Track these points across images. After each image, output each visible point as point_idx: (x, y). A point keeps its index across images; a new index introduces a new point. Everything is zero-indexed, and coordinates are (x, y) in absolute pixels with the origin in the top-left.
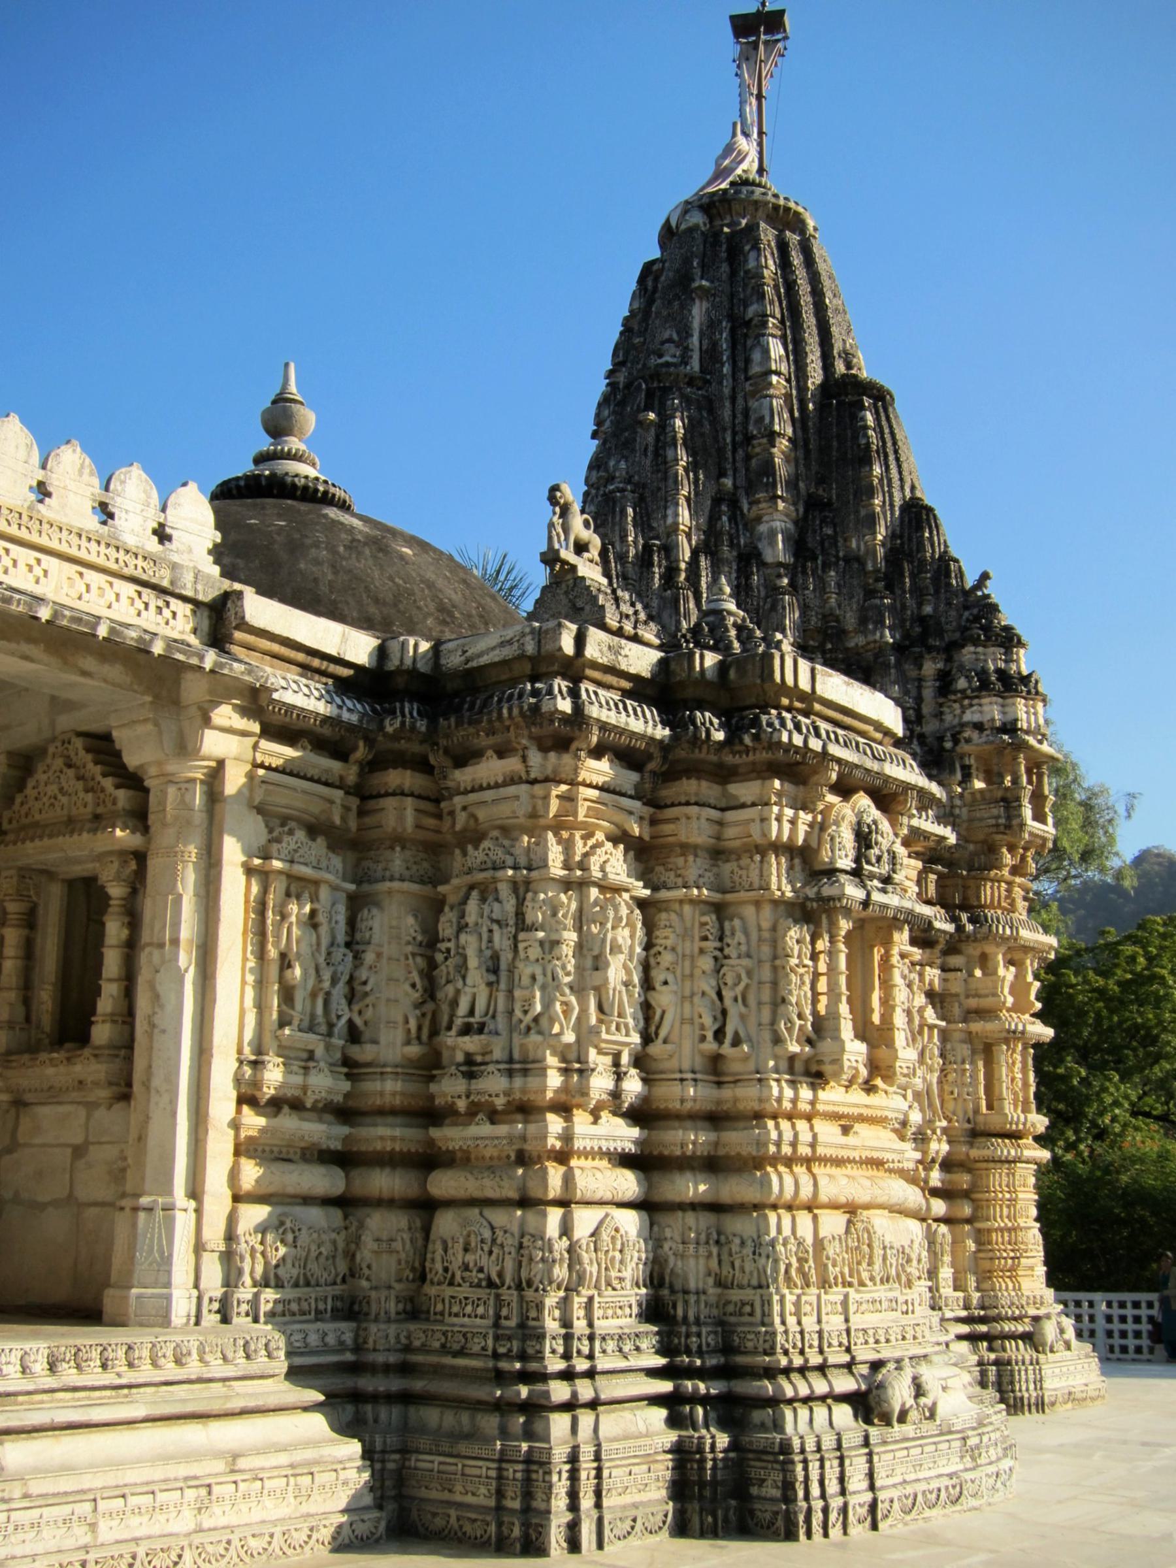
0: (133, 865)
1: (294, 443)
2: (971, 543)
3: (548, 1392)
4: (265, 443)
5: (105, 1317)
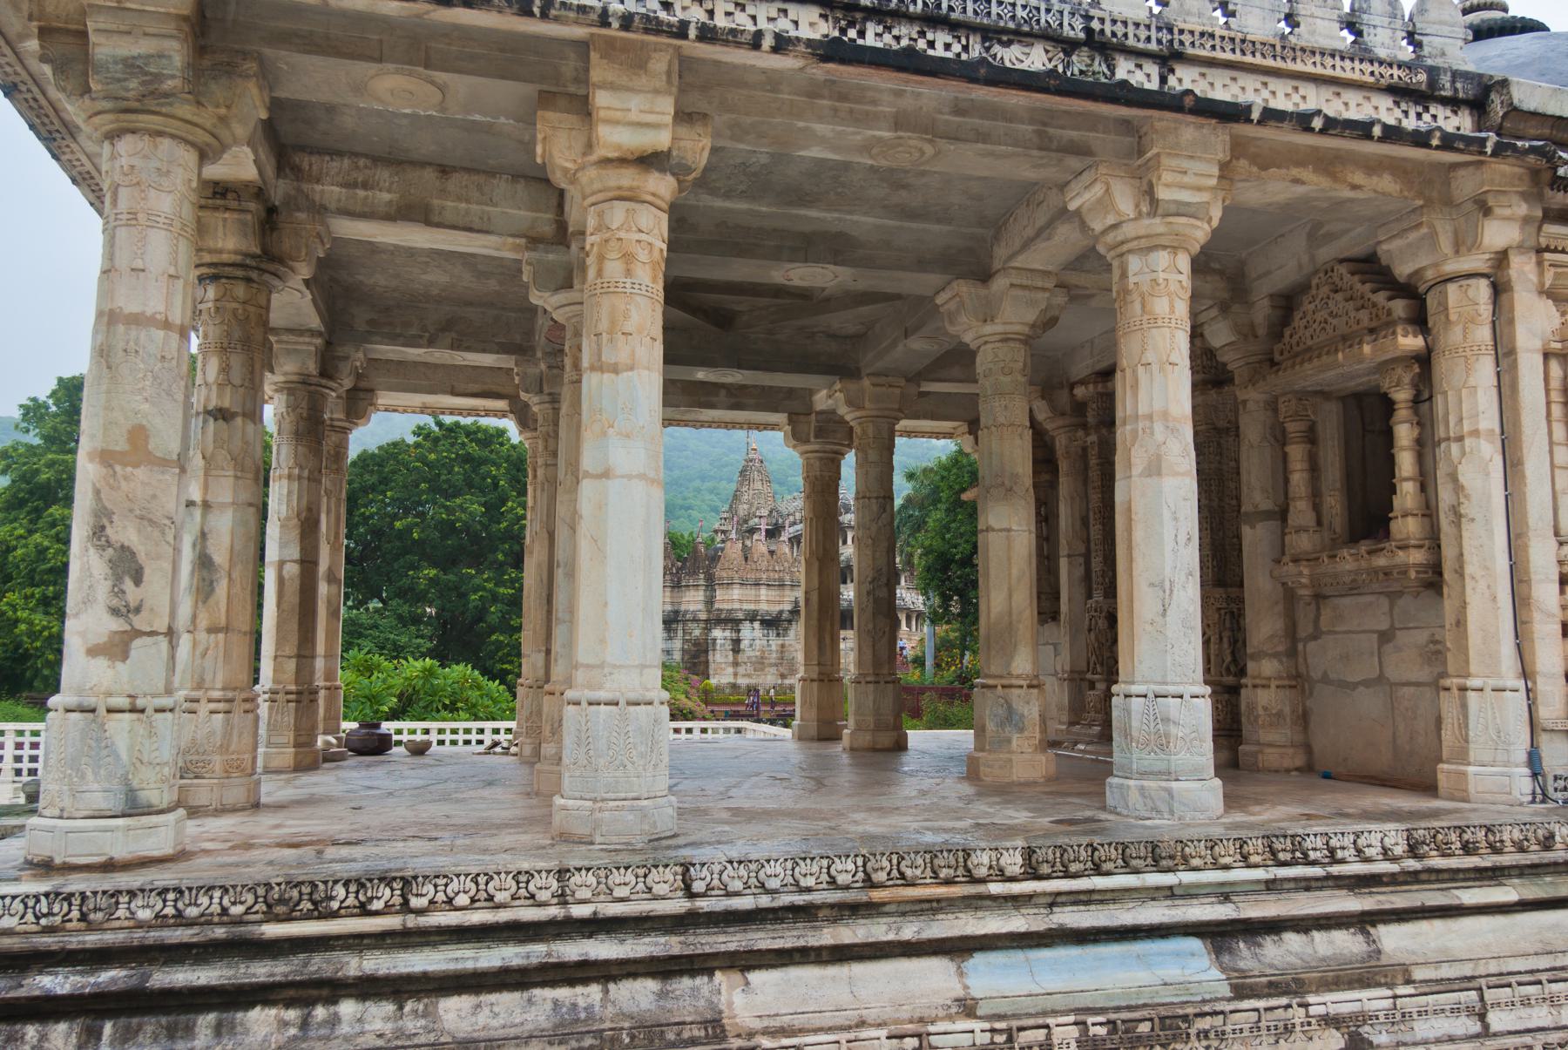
0: (1416, 369)
3: (53, 394)
5: (1441, 791)
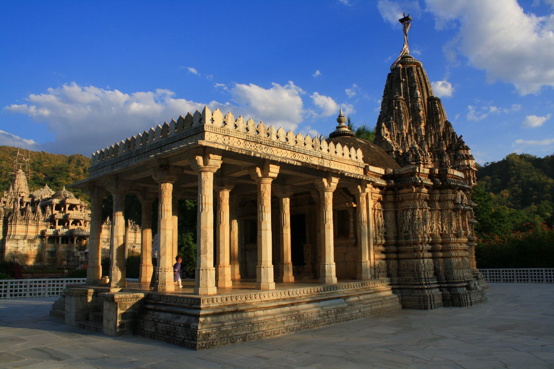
1: (343, 124)
2: (458, 130)
4: (337, 124)
